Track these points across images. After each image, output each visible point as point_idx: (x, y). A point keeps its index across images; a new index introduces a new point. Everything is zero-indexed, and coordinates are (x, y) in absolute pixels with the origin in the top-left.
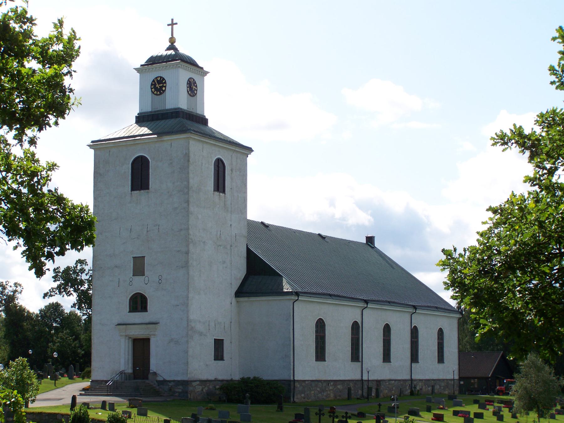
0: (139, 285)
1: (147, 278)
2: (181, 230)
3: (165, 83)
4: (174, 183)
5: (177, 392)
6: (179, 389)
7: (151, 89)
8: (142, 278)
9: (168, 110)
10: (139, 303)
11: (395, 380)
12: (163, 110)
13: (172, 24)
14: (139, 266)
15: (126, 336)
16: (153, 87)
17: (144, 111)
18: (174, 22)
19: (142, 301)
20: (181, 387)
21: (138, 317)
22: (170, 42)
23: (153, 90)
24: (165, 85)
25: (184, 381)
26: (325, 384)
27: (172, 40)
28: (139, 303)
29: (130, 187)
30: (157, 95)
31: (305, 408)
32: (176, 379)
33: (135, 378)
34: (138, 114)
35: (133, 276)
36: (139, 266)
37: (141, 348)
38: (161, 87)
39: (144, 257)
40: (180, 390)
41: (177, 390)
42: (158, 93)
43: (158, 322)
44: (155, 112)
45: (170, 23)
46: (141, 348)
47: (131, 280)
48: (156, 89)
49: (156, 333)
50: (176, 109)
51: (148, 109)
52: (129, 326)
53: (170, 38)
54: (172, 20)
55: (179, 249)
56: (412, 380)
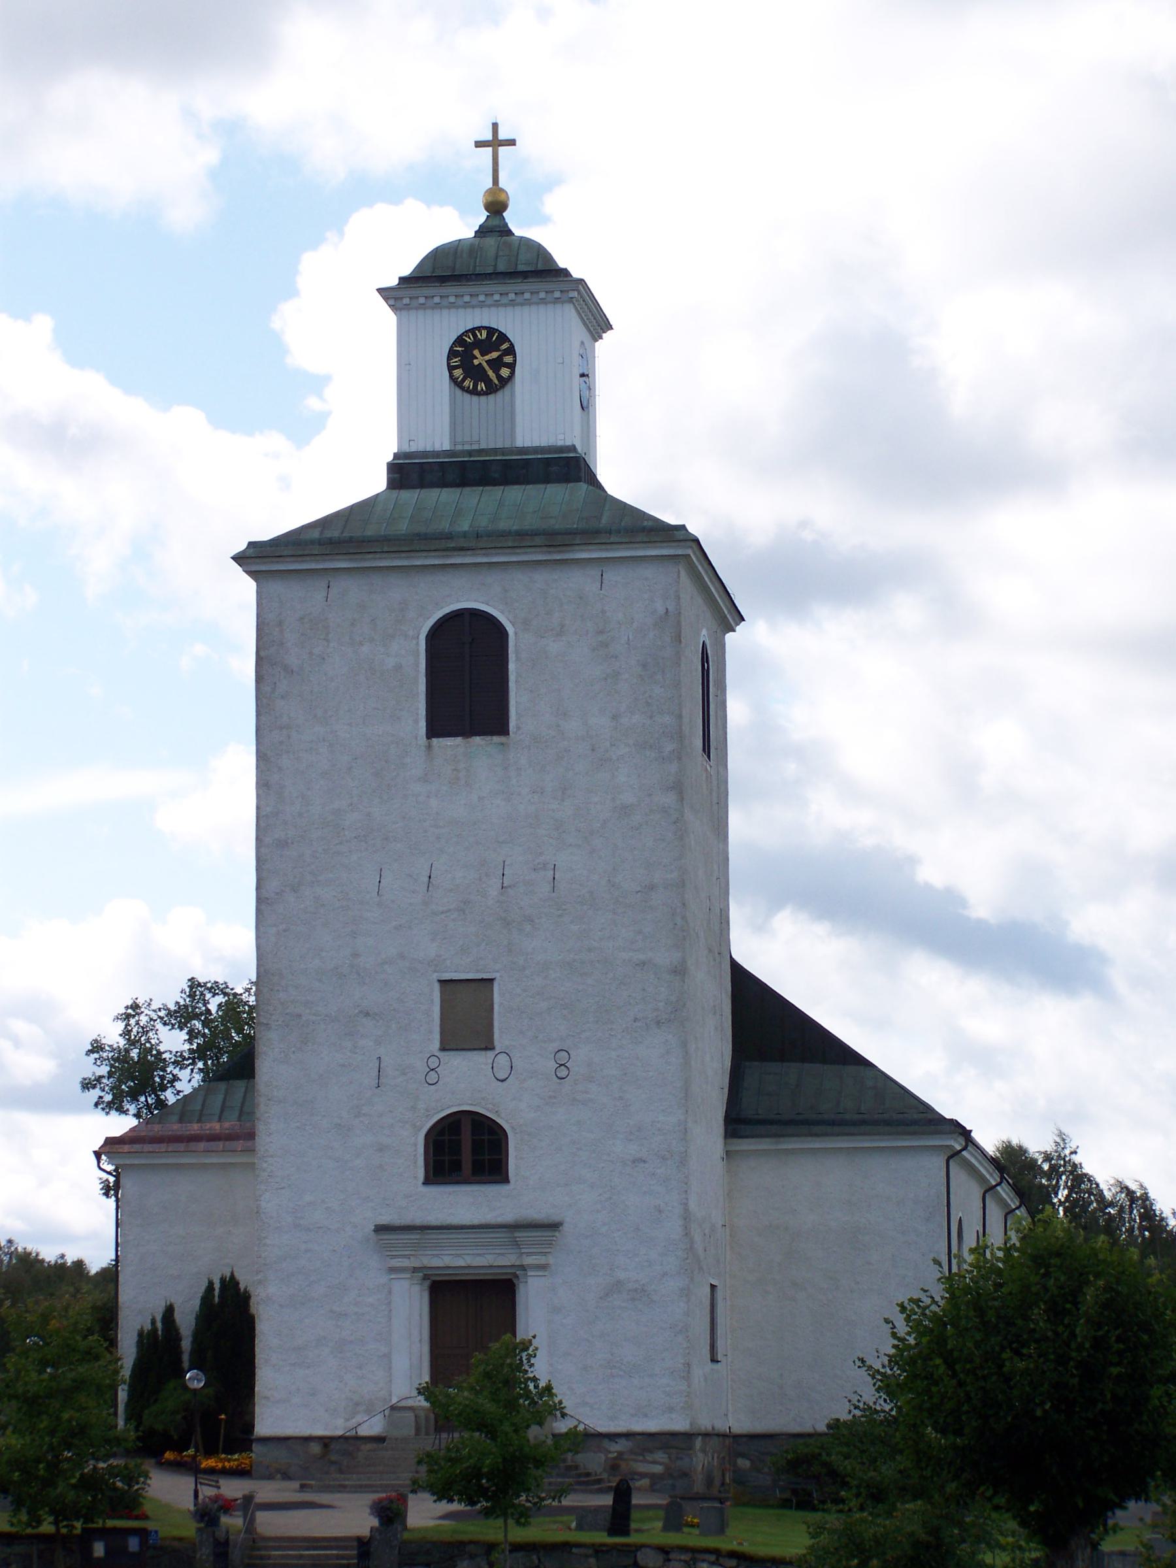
0: (466, 1084)
1: (503, 1060)
2: (652, 887)
3: (511, 351)
4: (615, 717)
5: (643, 1475)
6: (655, 1464)
7: (451, 369)
8: (480, 1059)
9: (523, 450)
10: (467, 1149)
11: (628, 1435)
12: (503, 451)
13: (495, 142)
14: (467, 1016)
15: (415, 1270)
16: (455, 361)
17: (421, 444)
18: (502, 136)
19: (477, 1147)
20: (660, 1456)
21: (465, 1203)
22: (488, 207)
23: (458, 373)
24: (508, 359)
25: (674, 1435)
26: (316, 1449)
27: (496, 206)
28: (467, 1149)
29: (423, 724)
30: (474, 392)
31: (625, 1532)
32: (637, 1427)
33: (438, 1429)
34: (396, 456)
35: (443, 1049)
36: (467, 1016)
37: (473, 1312)
38: (496, 364)
39: (492, 980)
40: (658, 1469)
41: (642, 1468)
42: (482, 386)
43: (556, 1218)
44: (470, 453)
45: (489, 136)
46: (473, 1312)
47: (433, 1062)
48: (477, 374)
49: (551, 1260)
50: (561, 449)
51: (437, 439)
52: (433, 1235)
53: (489, 191)
54: (495, 126)
55: (642, 957)
56: (252, 1441)
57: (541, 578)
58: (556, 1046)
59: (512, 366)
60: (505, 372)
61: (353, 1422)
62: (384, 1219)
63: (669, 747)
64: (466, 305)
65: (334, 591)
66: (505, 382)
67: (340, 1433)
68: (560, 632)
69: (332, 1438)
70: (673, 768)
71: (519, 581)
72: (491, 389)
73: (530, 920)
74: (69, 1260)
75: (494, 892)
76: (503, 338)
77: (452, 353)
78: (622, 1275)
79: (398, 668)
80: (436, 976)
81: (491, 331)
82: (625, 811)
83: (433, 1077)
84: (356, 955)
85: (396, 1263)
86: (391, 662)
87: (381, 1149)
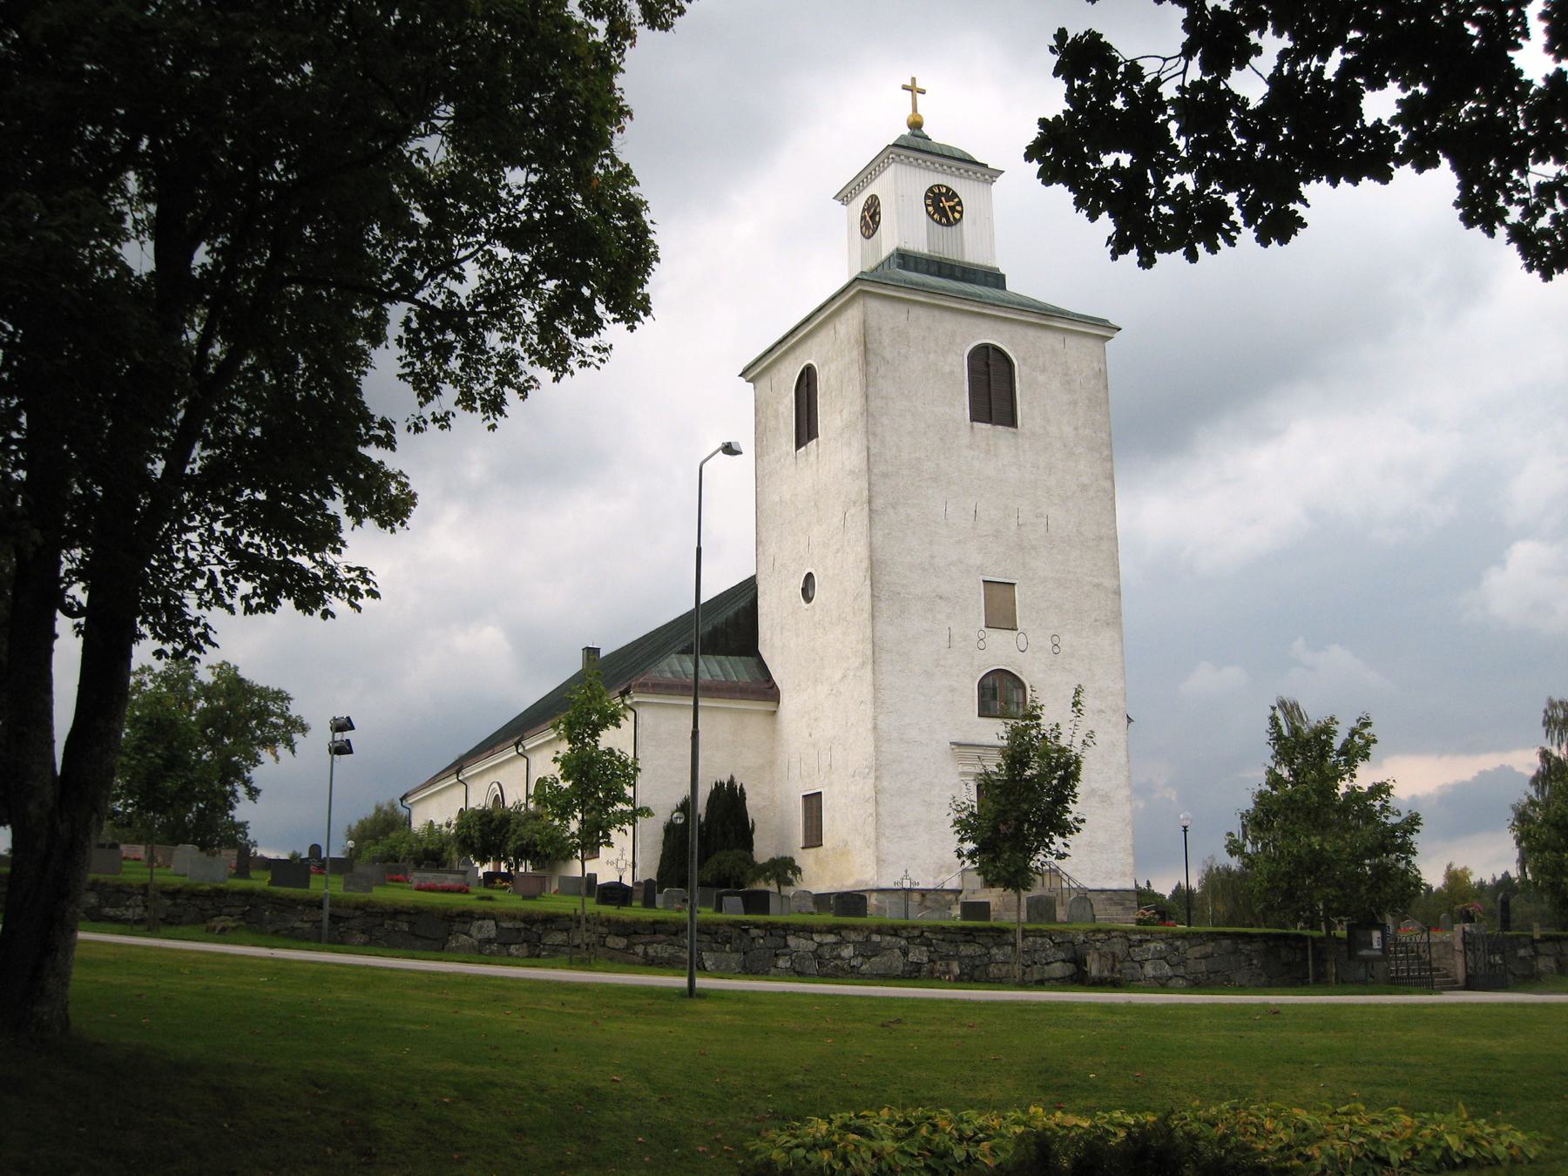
0: (1001, 651)
3: (960, 203)
11: (1103, 891)
14: (1000, 605)
30: (939, 222)
32: (1107, 886)
36: (1000, 605)
38: (953, 209)
48: (942, 212)
57: (1032, 333)
58: (1052, 632)
59: (961, 213)
60: (957, 215)
61: (939, 880)
62: (956, 739)
63: (1106, 453)
64: (935, 170)
65: (912, 315)
66: (957, 221)
67: (931, 887)
68: (1044, 370)
69: (929, 890)
70: (1109, 465)
71: (1020, 331)
72: (949, 224)
73: (1034, 548)
74: (1499, 877)
75: (1014, 527)
76: (955, 195)
77: (927, 197)
78: (1094, 786)
79: (952, 372)
80: (981, 578)
81: (948, 189)
82: (1084, 488)
83: (982, 645)
84: (932, 557)
85: (966, 769)
86: (947, 369)
87: (953, 690)
